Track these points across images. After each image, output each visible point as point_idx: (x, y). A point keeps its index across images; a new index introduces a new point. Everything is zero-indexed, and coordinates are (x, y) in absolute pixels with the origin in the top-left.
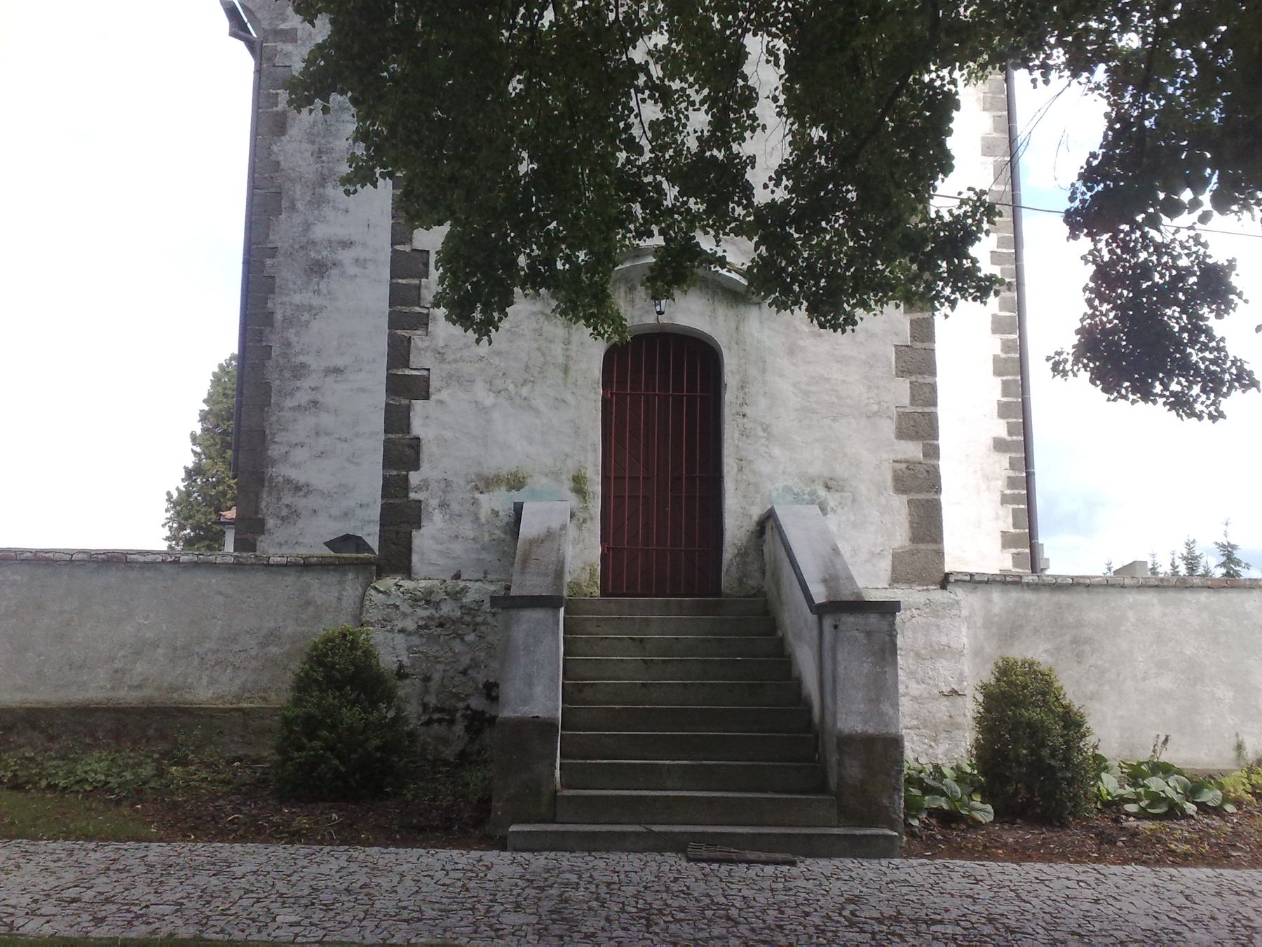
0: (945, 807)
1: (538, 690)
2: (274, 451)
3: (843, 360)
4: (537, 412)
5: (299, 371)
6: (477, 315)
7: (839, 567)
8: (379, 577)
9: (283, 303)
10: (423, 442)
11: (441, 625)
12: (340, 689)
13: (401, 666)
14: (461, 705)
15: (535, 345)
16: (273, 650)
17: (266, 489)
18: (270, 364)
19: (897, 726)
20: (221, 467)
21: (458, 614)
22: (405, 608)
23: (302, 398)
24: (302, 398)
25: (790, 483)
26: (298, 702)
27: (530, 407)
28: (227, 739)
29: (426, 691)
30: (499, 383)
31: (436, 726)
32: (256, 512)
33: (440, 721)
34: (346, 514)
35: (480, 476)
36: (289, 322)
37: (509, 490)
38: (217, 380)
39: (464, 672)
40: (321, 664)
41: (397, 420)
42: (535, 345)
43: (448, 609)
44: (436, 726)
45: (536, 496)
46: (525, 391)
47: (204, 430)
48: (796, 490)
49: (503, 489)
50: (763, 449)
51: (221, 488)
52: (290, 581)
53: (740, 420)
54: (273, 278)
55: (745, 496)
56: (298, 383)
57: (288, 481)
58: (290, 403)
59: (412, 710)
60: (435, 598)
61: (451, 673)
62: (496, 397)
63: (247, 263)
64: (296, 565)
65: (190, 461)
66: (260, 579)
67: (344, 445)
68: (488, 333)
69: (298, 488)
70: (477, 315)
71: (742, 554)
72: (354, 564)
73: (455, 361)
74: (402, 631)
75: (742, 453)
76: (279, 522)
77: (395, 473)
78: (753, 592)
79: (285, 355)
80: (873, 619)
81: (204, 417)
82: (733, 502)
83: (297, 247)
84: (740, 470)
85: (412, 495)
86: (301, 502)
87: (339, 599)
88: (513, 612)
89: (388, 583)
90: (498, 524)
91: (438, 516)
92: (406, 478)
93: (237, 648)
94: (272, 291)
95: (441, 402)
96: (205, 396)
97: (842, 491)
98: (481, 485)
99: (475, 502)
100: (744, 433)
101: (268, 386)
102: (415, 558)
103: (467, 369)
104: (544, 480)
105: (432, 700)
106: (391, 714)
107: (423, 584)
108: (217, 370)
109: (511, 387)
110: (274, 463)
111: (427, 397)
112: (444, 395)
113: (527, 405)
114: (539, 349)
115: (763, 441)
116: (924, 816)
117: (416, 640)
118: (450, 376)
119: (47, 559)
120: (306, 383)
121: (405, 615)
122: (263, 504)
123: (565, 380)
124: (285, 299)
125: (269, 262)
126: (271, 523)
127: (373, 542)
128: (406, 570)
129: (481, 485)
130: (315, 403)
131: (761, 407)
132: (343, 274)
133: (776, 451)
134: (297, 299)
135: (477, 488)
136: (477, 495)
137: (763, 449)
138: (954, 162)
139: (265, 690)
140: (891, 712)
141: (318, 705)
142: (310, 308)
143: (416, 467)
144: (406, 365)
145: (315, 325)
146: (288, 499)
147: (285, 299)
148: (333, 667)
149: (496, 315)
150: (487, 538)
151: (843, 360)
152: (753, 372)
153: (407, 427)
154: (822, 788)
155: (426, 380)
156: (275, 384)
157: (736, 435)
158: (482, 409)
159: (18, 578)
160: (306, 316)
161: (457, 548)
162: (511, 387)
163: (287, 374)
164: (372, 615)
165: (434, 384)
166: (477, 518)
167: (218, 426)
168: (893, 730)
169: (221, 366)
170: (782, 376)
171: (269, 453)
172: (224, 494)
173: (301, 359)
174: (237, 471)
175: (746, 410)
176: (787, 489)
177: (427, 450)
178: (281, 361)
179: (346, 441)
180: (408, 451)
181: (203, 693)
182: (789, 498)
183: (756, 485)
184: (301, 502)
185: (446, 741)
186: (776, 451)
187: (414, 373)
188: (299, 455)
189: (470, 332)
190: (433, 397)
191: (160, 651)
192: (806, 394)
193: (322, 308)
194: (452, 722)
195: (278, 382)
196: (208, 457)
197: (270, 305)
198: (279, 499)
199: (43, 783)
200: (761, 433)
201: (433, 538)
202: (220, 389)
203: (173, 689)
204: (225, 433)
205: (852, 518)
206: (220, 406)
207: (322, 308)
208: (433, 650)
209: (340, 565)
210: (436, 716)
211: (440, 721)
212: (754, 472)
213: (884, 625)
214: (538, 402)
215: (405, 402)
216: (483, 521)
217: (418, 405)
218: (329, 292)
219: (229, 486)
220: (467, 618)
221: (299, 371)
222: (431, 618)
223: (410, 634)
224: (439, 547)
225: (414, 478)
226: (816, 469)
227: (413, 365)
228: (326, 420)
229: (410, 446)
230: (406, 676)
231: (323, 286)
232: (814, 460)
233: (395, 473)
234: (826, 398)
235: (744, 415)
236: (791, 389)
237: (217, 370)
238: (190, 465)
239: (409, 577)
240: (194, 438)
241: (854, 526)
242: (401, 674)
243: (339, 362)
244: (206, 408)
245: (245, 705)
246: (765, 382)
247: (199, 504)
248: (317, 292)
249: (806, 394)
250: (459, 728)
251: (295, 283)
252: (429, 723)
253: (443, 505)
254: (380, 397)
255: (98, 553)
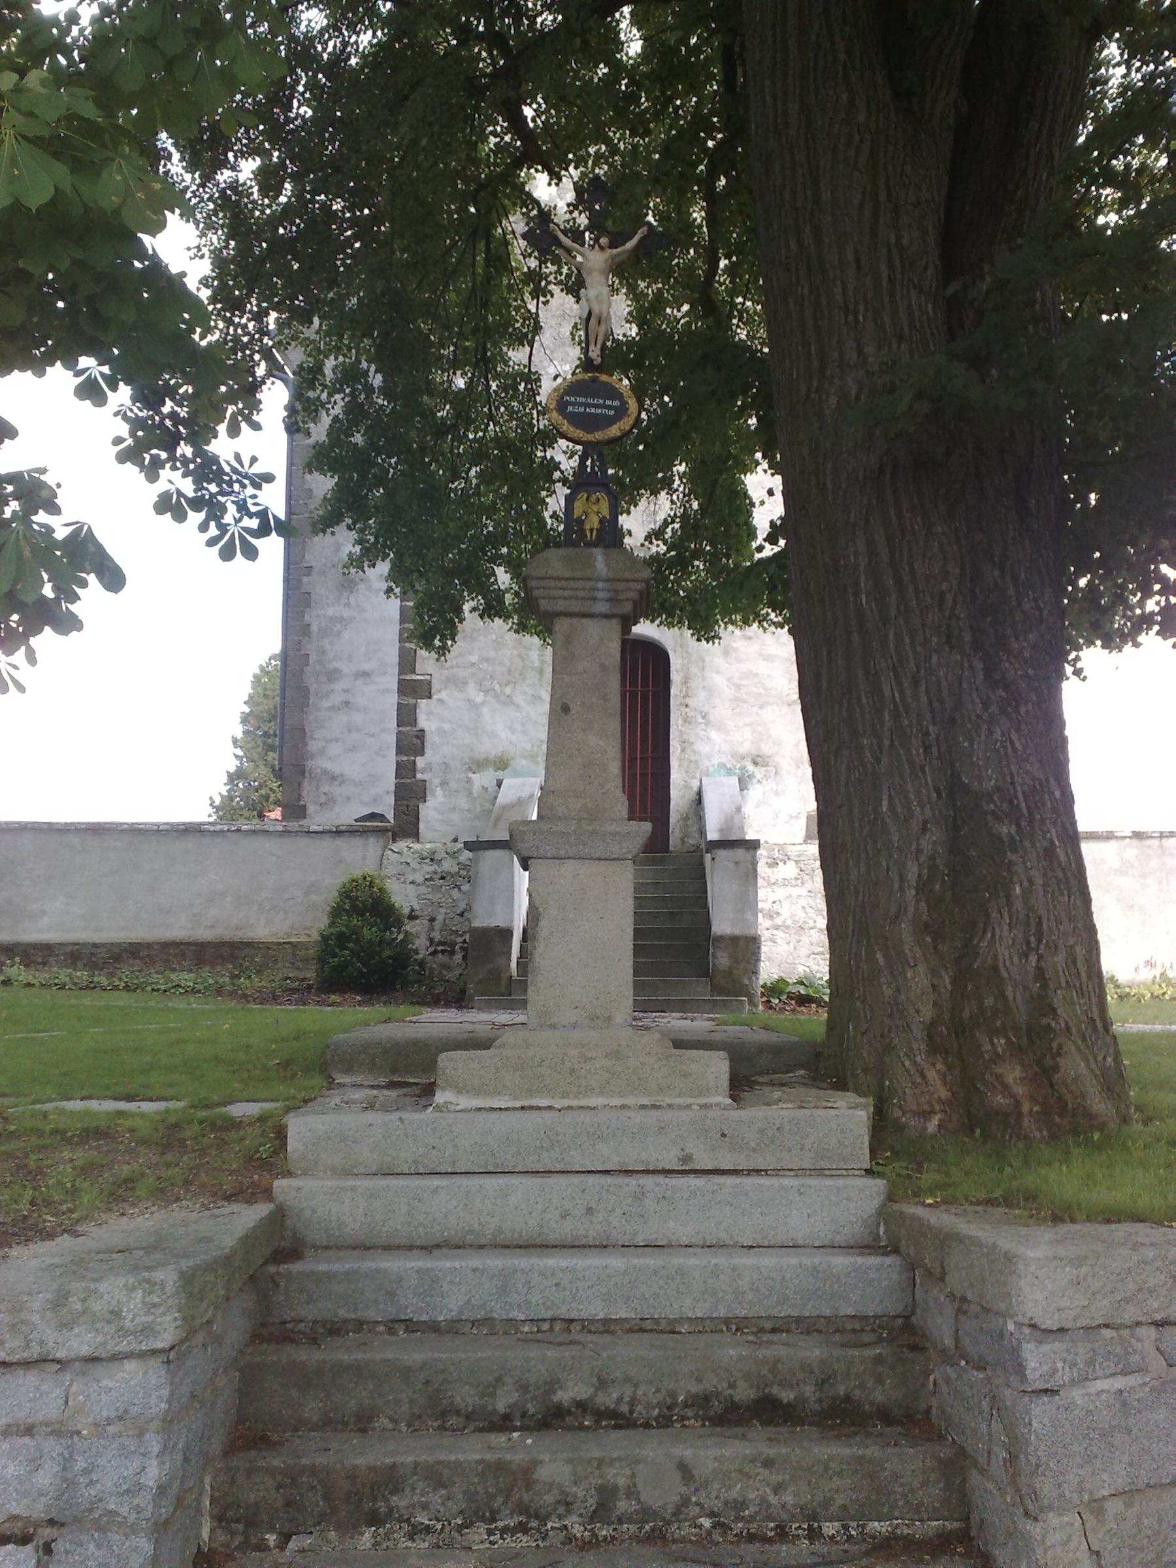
0: (802, 992)
1: (499, 907)
2: (313, 746)
3: (768, 658)
4: (518, 706)
5: (333, 676)
6: (437, 643)
7: (736, 821)
8: (394, 840)
9: (318, 616)
10: (427, 733)
11: (443, 878)
12: (362, 915)
13: (412, 910)
14: (460, 940)
15: (515, 652)
16: (314, 897)
17: (306, 780)
18: (308, 669)
19: (756, 929)
20: (264, 770)
21: (456, 869)
22: (414, 864)
23: (336, 699)
24: (336, 699)
25: (724, 760)
26: (332, 925)
27: (512, 703)
28: (280, 965)
29: (432, 929)
30: (487, 684)
31: (440, 956)
32: (299, 799)
33: (443, 952)
34: (375, 800)
35: (472, 760)
36: (323, 632)
37: (496, 771)
38: (257, 681)
39: (461, 915)
40: (348, 897)
41: (407, 716)
42: (515, 652)
43: (448, 865)
44: (440, 956)
45: (516, 774)
46: (508, 690)
47: (246, 733)
48: (729, 766)
49: (491, 770)
50: (702, 733)
51: (263, 792)
52: (327, 843)
53: (684, 710)
54: (308, 593)
55: (687, 772)
56: (332, 686)
57: (325, 772)
58: (326, 704)
59: (420, 944)
60: (437, 857)
61: (452, 915)
62: (485, 695)
63: (287, 580)
64: (331, 832)
65: (232, 765)
66: (303, 842)
67: (372, 740)
68: (444, 654)
69: (333, 778)
70: (437, 643)
71: (685, 818)
72: (374, 831)
73: (452, 667)
74: (412, 883)
75: (685, 737)
76: (318, 808)
77: (405, 758)
78: (692, 849)
79: (320, 662)
80: (740, 853)
81: (245, 719)
82: (677, 776)
83: (329, 565)
84: (683, 750)
85: (419, 776)
86: (336, 790)
87: (364, 858)
88: (481, 852)
89: (402, 845)
90: (487, 797)
91: (439, 793)
92: (414, 762)
93: (286, 896)
94: (309, 606)
95: (441, 701)
96: (246, 698)
97: (767, 765)
98: (474, 767)
99: (469, 781)
100: (687, 720)
101: (307, 688)
102: (421, 826)
103: (462, 673)
104: (524, 762)
105: (437, 936)
106: (401, 937)
107: (428, 846)
108: (258, 671)
109: (497, 687)
110: (313, 757)
111: (430, 697)
112: (443, 695)
113: (509, 701)
114: (519, 655)
115: (703, 726)
116: (784, 997)
117: (423, 890)
118: (448, 679)
119: (140, 830)
120: (339, 686)
121: (414, 870)
122: (304, 793)
123: (540, 680)
124: (321, 612)
125: (305, 579)
126: (311, 809)
127: (390, 816)
128: (415, 835)
129: (474, 767)
130: (347, 703)
131: (699, 699)
132: (369, 588)
133: (713, 734)
134: (330, 611)
135: (470, 769)
136: (471, 775)
137: (702, 733)
138: (239, 731)
139: (309, 929)
140: (752, 919)
141: (347, 926)
142: (341, 620)
143: (422, 753)
144: (414, 672)
145: (346, 635)
146: (325, 788)
147: (321, 612)
148: (357, 899)
149: (449, 642)
150: (478, 809)
151: (768, 658)
152: (694, 669)
153: (414, 722)
154: (706, 975)
155: (429, 683)
156: (313, 688)
157: (680, 722)
158: (474, 706)
159: (119, 844)
160: (338, 627)
161: (455, 817)
162: (497, 687)
163: (323, 679)
164: (389, 870)
165: (435, 686)
166: (470, 793)
167: (259, 728)
168: (752, 932)
169: (262, 668)
170: (718, 672)
171: (309, 748)
172: (267, 798)
173: (337, 664)
174: (278, 774)
175: (688, 701)
176: (722, 765)
177: (431, 739)
178: (318, 667)
179: (373, 736)
180: (415, 741)
181: (263, 930)
182: (723, 772)
183: (696, 762)
184: (336, 790)
185: (447, 967)
186: (713, 734)
187: (419, 677)
188: (334, 749)
189: (433, 653)
190: (435, 697)
191: (228, 899)
192: (738, 687)
193: (352, 619)
194: (452, 953)
195: (315, 686)
196: (250, 760)
197: (307, 617)
198: (318, 788)
199: (149, 988)
200: (700, 720)
201: (436, 809)
202: (260, 690)
203: (237, 928)
204: (266, 734)
205: (775, 787)
206: (261, 708)
207: (352, 619)
208: (436, 897)
209: (365, 832)
210: (439, 948)
211: (443, 952)
212: (694, 752)
213: (748, 856)
214: (519, 699)
215: (412, 701)
216: (475, 795)
217: (423, 703)
218: (358, 606)
219: (271, 789)
220: (463, 873)
221: (333, 676)
222: (435, 872)
223: (419, 885)
224: (440, 817)
225: (420, 762)
226: (746, 747)
227: (417, 671)
228: (357, 718)
229: (417, 737)
230: (416, 917)
231: (352, 600)
232: (744, 741)
233: (405, 758)
234: (755, 689)
235: (687, 706)
236: (726, 683)
237: (258, 671)
238: (232, 769)
239: (418, 841)
240: (235, 741)
241: (777, 793)
242: (412, 917)
243: (367, 666)
244: (247, 710)
245: (292, 940)
246: (704, 678)
247: (241, 809)
248: (348, 605)
249: (738, 687)
250: (458, 957)
251: (328, 598)
252: (434, 953)
253: (444, 784)
254: (393, 698)
255: (178, 824)
